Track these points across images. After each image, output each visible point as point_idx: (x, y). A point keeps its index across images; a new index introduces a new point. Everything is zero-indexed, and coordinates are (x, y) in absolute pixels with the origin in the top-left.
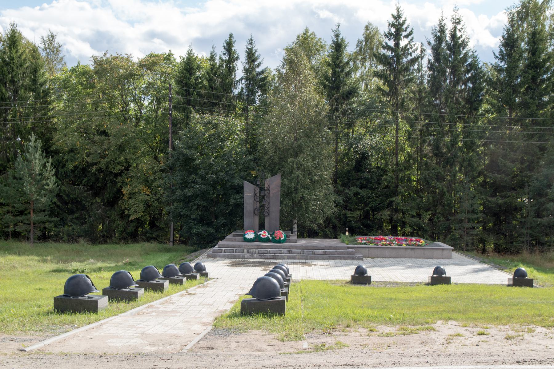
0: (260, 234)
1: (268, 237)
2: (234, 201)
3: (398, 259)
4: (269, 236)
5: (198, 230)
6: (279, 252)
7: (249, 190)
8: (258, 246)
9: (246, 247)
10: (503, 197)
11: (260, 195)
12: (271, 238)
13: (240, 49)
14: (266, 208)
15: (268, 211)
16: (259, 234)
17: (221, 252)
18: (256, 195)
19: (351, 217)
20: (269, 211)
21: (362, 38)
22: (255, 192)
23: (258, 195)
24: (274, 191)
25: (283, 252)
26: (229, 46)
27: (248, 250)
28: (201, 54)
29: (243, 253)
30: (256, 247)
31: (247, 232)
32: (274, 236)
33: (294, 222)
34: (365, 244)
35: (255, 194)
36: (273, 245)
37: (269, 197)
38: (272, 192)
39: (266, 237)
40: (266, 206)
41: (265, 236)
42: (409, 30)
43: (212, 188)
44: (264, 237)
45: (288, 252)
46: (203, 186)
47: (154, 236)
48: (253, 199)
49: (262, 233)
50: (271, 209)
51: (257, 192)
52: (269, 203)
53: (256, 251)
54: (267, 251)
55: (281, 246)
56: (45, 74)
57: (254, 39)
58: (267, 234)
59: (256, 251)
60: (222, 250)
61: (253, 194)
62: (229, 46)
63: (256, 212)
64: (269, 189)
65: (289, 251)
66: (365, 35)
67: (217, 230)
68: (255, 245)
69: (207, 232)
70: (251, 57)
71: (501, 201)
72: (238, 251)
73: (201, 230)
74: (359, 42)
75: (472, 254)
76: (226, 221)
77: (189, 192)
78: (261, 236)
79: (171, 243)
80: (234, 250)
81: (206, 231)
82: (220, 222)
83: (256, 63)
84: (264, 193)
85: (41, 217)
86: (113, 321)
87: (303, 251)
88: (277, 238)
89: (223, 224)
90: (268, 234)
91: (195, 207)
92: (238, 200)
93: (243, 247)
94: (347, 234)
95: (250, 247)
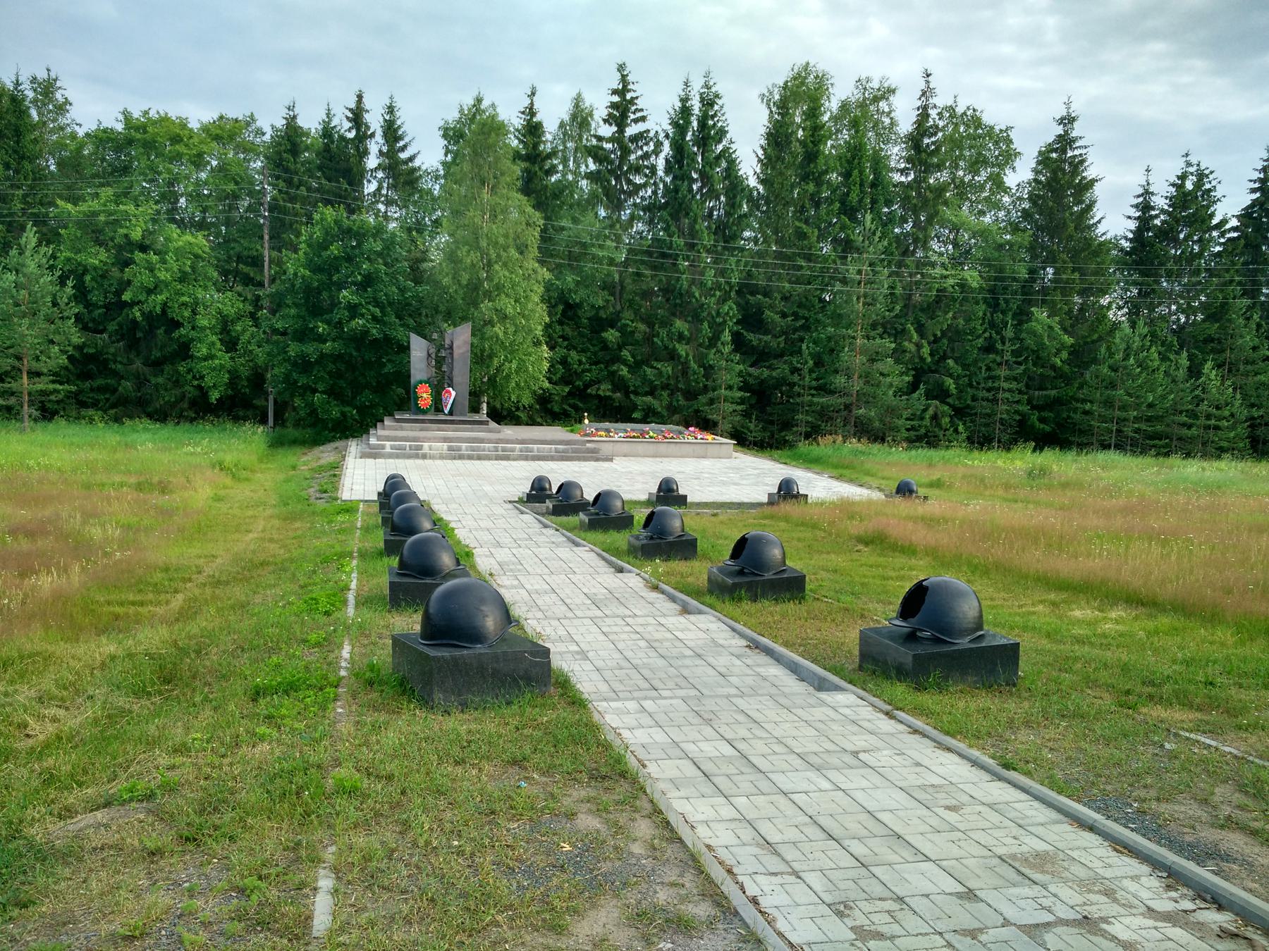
3: (658, 459)
7: (419, 349)
10: (770, 368)
11: (437, 356)
13: (374, 120)
21: (567, 118)
23: (433, 356)
24: (461, 351)
26: (357, 116)
28: (310, 122)
34: (672, 438)
35: (429, 355)
42: (639, 115)
57: (397, 104)
61: (425, 354)
62: (357, 116)
66: (506, 122)
67: (362, 410)
70: (392, 132)
71: (766, 373)
74: (562, 125)
75: (777, 453)
77: (310, 349)
83: (401, 143)
85: (42, 385)
86: (761, 670)
94: (586, 421)
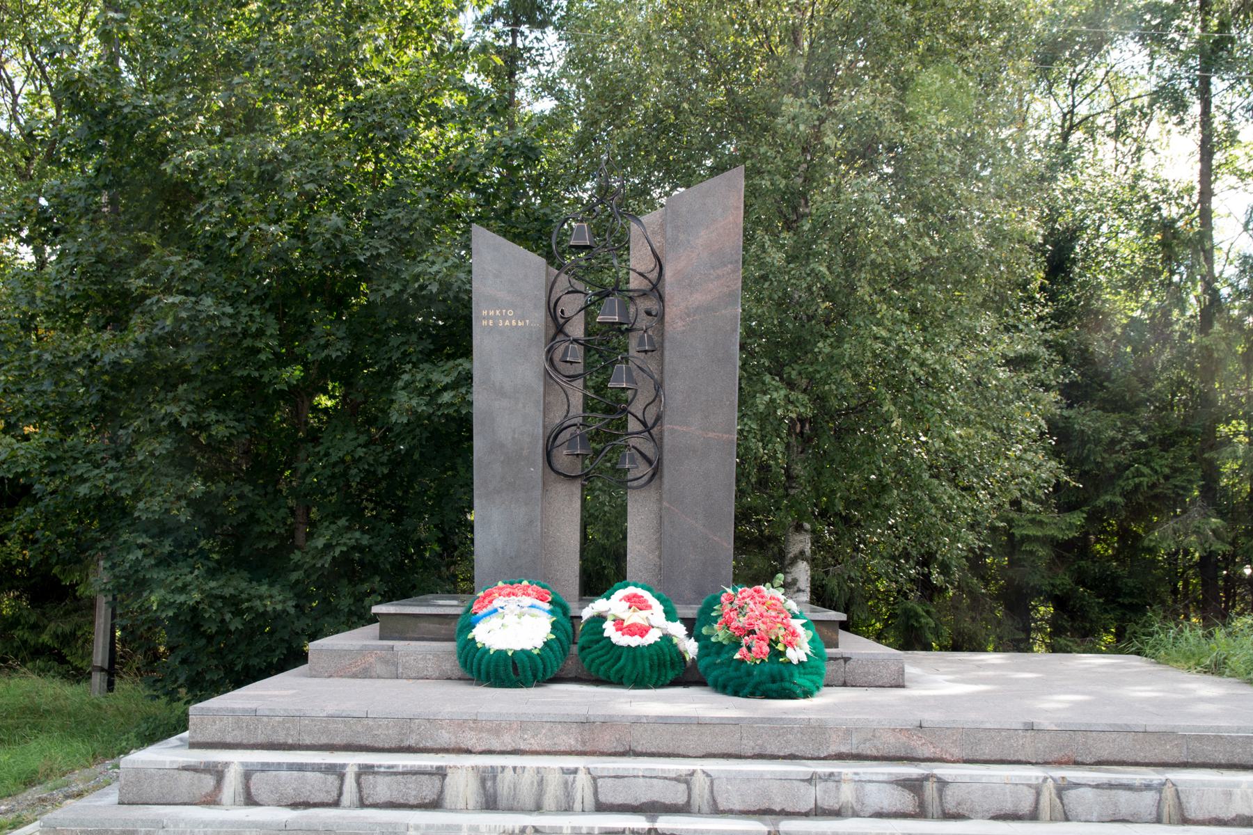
0: (600, 619)
1: (667, 638)
2: (419, 404)
4: (678, 630)
5: (181, 598)
6: (808, 797)
8: (585, 724)
9: (470, 740)
12: (691, 648)
14: (633, 425)
15: (648, 448)
16: (587, 613)
17: (211, 800)
18: (560, 330)
19: (1036, 539)
20: (658, 444)
22: (552, 309)
24: (698, 298)
25: (847, 794)
27: (487, 778)
29: (435, 804)
30: (570, 742)
31: (489, 597)
32: (719, 634)
33: (793, 550)
35: (557, 324)
36: (736, 722)
37: (655, 348)
38: (678, 303)
39: (652, 637)
40: (636, 408)
41: (643, 631)
43: (271, 319)
44: (634, 641)
45: (905, 800)
46: (208, 301)
47: (45, 638)
48: (538, 356)
49: (613, 605)
50: (672, 430)
51: (571, 305)
52: (659, 386)
53: (568, 789)
54: (686, 780)
55: (778, 726)
56: (196, 359)
58: (655, 615)
59: (568, 789)
60: (218, 772)
61: (537, 319)
63: (562, 457)
64: (655, 290)
65: (913, 786)
68: (566, 723)
69: (238, 613)
72: (382, 789)
73: (197, 596)
76: (365, 540)
78: (609, 629)
79: (98, 679)
80: (337, 771)
81: (234, 603)
82: (328, 547)
84: (624, 311)
87: (1062, 789)
88: (753, 652)
89: (345, 559)
90: (670, 615)
91: (162, 446)
92: (446, 397)
93: (445, 738)
95: (508, 741)
